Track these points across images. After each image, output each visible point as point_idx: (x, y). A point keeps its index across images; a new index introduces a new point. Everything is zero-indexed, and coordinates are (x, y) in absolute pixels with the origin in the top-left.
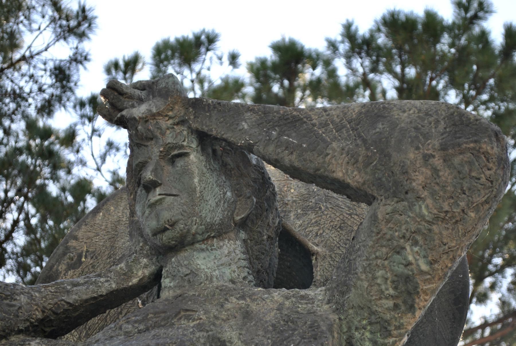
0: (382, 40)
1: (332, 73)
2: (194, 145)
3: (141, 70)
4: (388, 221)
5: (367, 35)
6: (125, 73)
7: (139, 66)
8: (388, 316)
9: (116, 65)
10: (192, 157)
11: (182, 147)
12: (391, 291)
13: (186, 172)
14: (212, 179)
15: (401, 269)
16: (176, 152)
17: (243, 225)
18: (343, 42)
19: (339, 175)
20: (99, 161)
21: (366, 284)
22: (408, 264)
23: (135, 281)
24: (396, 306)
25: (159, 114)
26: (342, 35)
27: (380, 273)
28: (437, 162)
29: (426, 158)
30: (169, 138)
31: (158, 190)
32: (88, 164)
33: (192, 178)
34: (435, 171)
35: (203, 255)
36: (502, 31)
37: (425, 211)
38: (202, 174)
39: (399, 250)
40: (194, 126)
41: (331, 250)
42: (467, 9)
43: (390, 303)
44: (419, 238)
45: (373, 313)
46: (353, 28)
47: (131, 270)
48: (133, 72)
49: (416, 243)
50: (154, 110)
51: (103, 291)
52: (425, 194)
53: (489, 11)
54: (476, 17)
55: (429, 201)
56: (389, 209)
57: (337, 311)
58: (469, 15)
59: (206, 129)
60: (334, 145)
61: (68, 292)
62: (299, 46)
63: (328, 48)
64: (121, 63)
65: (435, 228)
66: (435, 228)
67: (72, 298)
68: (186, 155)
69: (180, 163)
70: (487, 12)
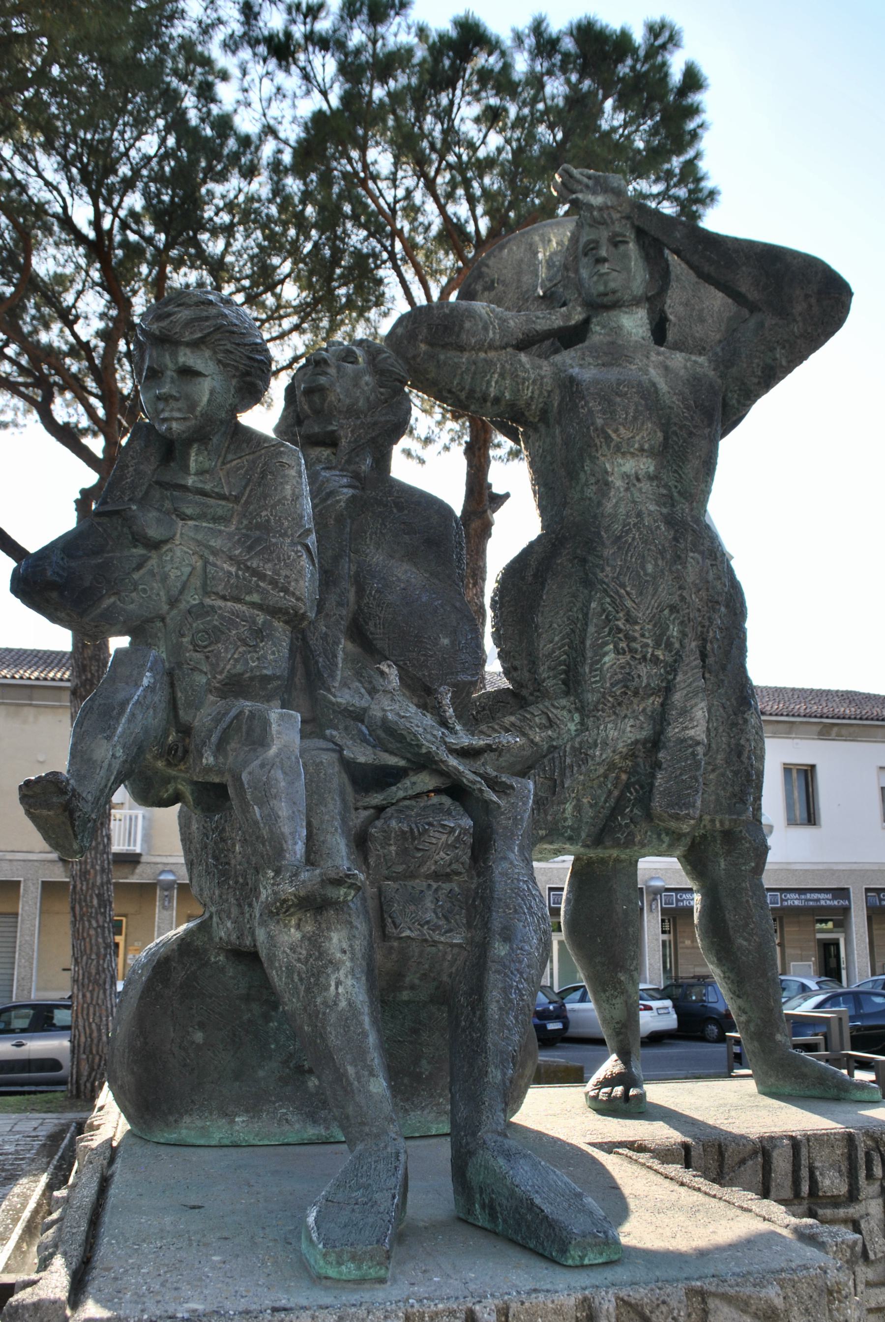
0: (568, 44)
1: (507, 67)
2: (633, 236)
3: (325, 17)
4: (770, 330)
5: (554, 36)
6: (305, 17)
7: (323, 14)
8: (752, 388)
9: (298, 6)
10: (631, 245)
11: (625, 236)
12: (759, 373)
13: (626, 256)
14: (641, 263)
15: (769, 361)
16: (620, 239)
17: (648, 299)
18: (529, 36)
19: (743, 289)
20: (265, 104)
21: (745, 365)
22: (775, 359)
23: (573, 322)
24: (759, 383)
25: (612, 207)
26: (529, 28)
27: (756, 361)
28: (813, 301)
29: (807, 296)
30: (617, 228)
31: (607, 265)
32: (253, 105)
33: (630, 262)
34: (810, 306)
35: (626, 316)
36: (683, 67)
37: (796, 330)
38: (636, 260)
39: (772, 350)
40: (637, 223)
41: (680, 320)
42: (656, 36)
43: (756, 380)
44: (787, 345)
45: (743, 384)
46: (544, 25)
47: (570, 314)
48: (315, 18)
49: (784, 348)
50: (609, 204)
51: (555, 326)
52: (799, 319)
53: (677, 45)
54: (663, 47)
55: (801, 324)
56: (773, 322)
57: (720, 377)
58: (657, 43)
59: (646, 228)
60: (744, 268)
61: (534, 322)
62: (482, 29)
63: (514, 40)
64: (304, 6)
65: (798, 341)
66: (798, 341)
67: (538, 327)
68: (627, 242)
69: (622, 248)
70: (675, 45)
